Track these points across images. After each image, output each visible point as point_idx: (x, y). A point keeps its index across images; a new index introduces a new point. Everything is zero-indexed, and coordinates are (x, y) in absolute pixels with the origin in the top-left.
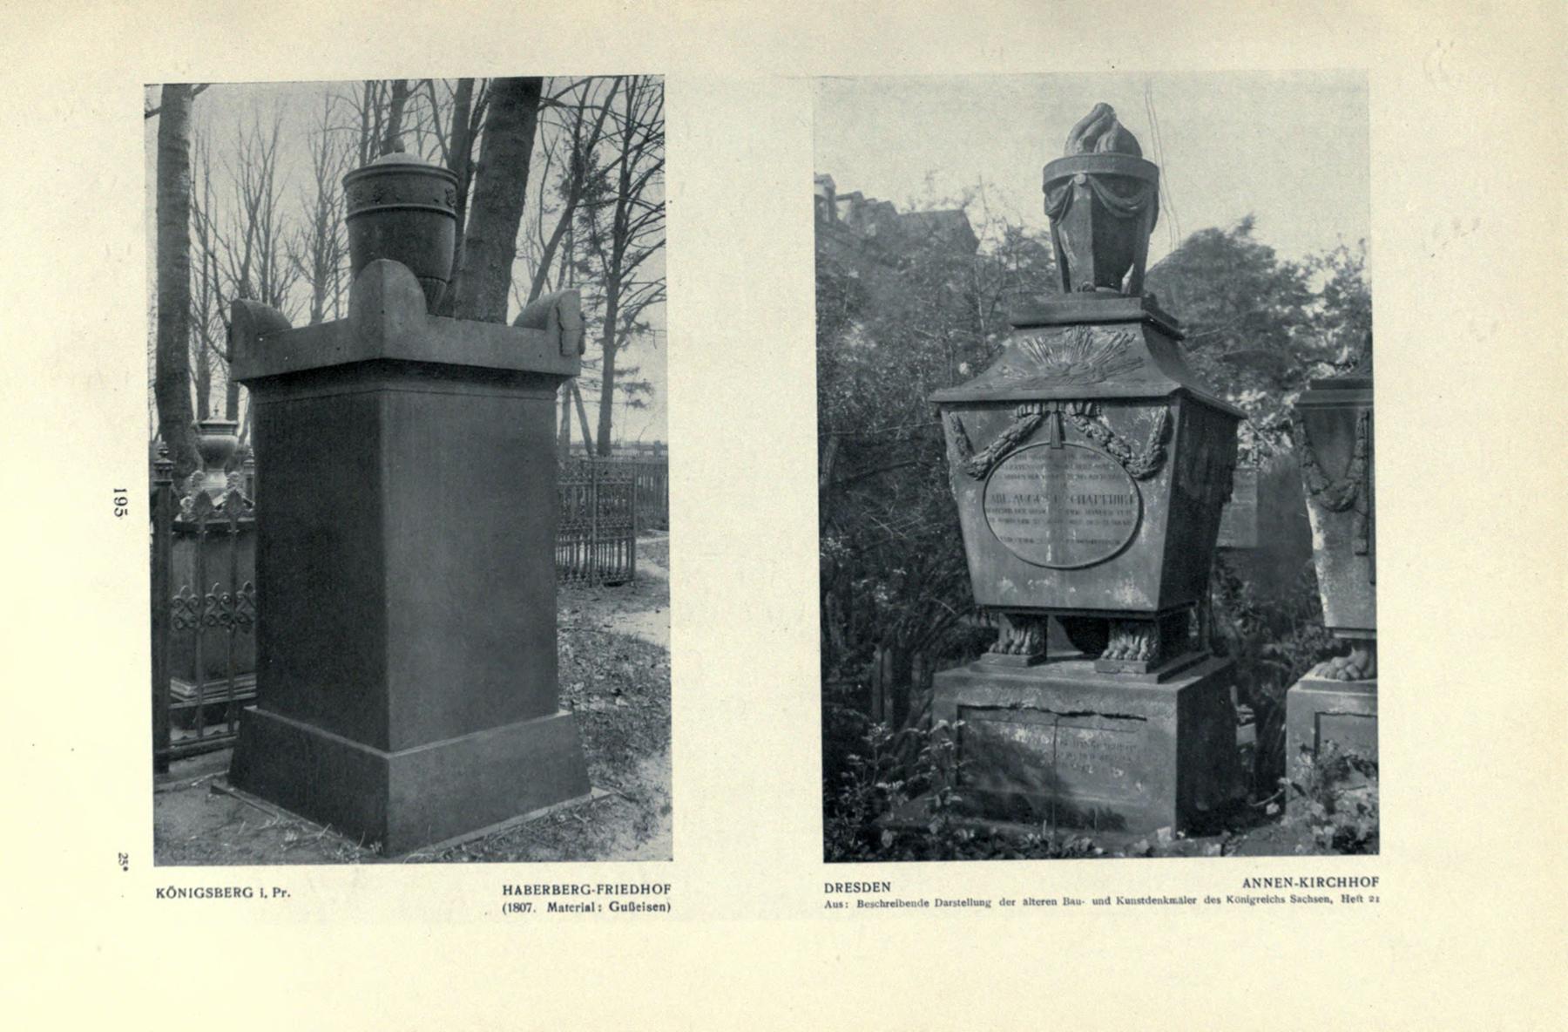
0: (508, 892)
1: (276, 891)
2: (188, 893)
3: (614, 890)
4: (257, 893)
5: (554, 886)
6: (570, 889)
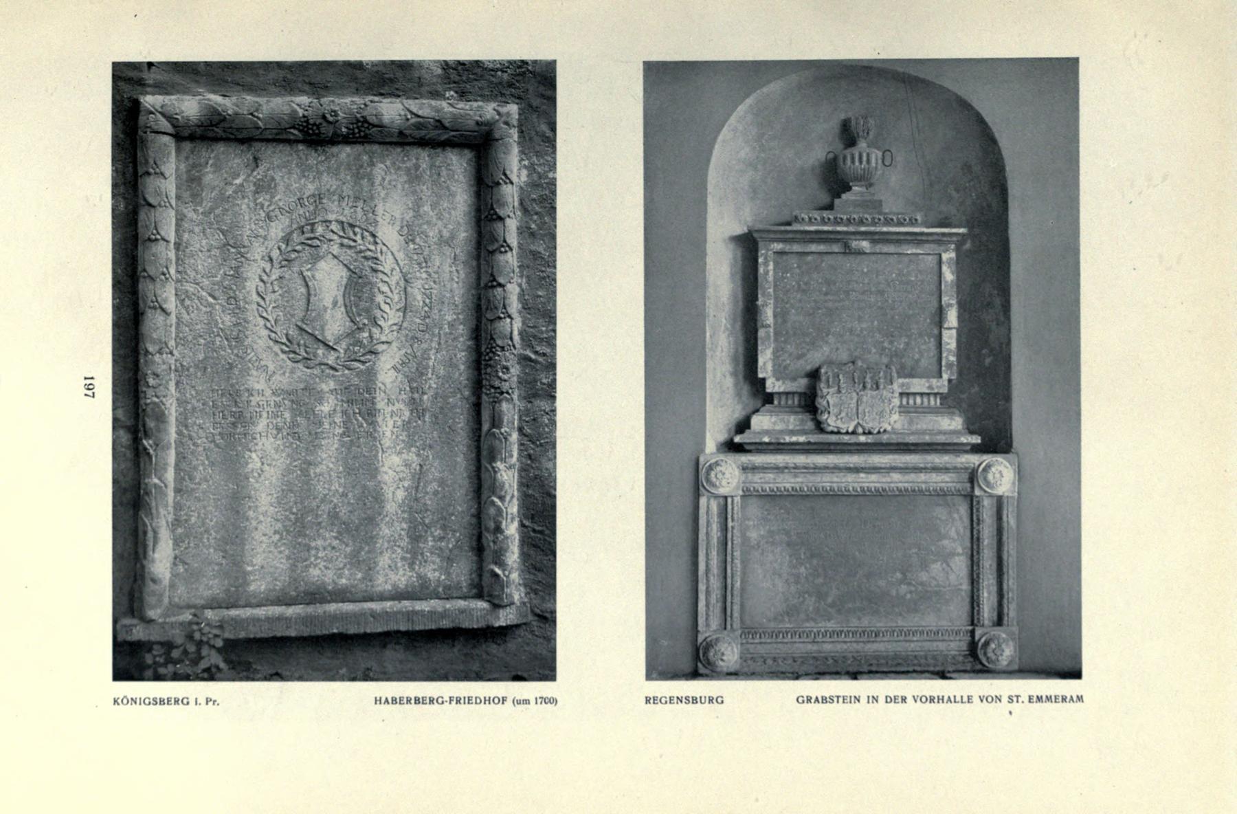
0: (378, 702)
1: (208, 701)
2: (138, 701)
3: (462, 701)
4: (192, 702)
5: (415, 698)
6: (428, 701)
